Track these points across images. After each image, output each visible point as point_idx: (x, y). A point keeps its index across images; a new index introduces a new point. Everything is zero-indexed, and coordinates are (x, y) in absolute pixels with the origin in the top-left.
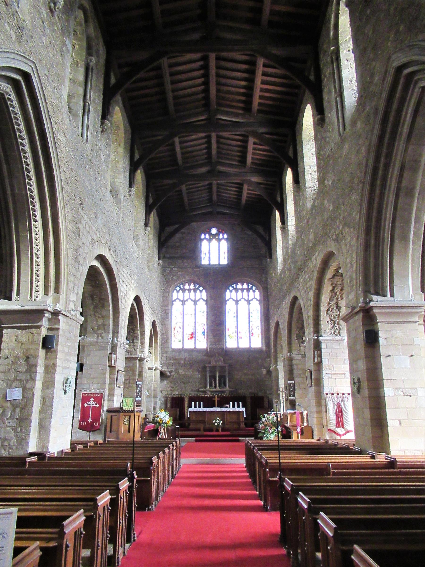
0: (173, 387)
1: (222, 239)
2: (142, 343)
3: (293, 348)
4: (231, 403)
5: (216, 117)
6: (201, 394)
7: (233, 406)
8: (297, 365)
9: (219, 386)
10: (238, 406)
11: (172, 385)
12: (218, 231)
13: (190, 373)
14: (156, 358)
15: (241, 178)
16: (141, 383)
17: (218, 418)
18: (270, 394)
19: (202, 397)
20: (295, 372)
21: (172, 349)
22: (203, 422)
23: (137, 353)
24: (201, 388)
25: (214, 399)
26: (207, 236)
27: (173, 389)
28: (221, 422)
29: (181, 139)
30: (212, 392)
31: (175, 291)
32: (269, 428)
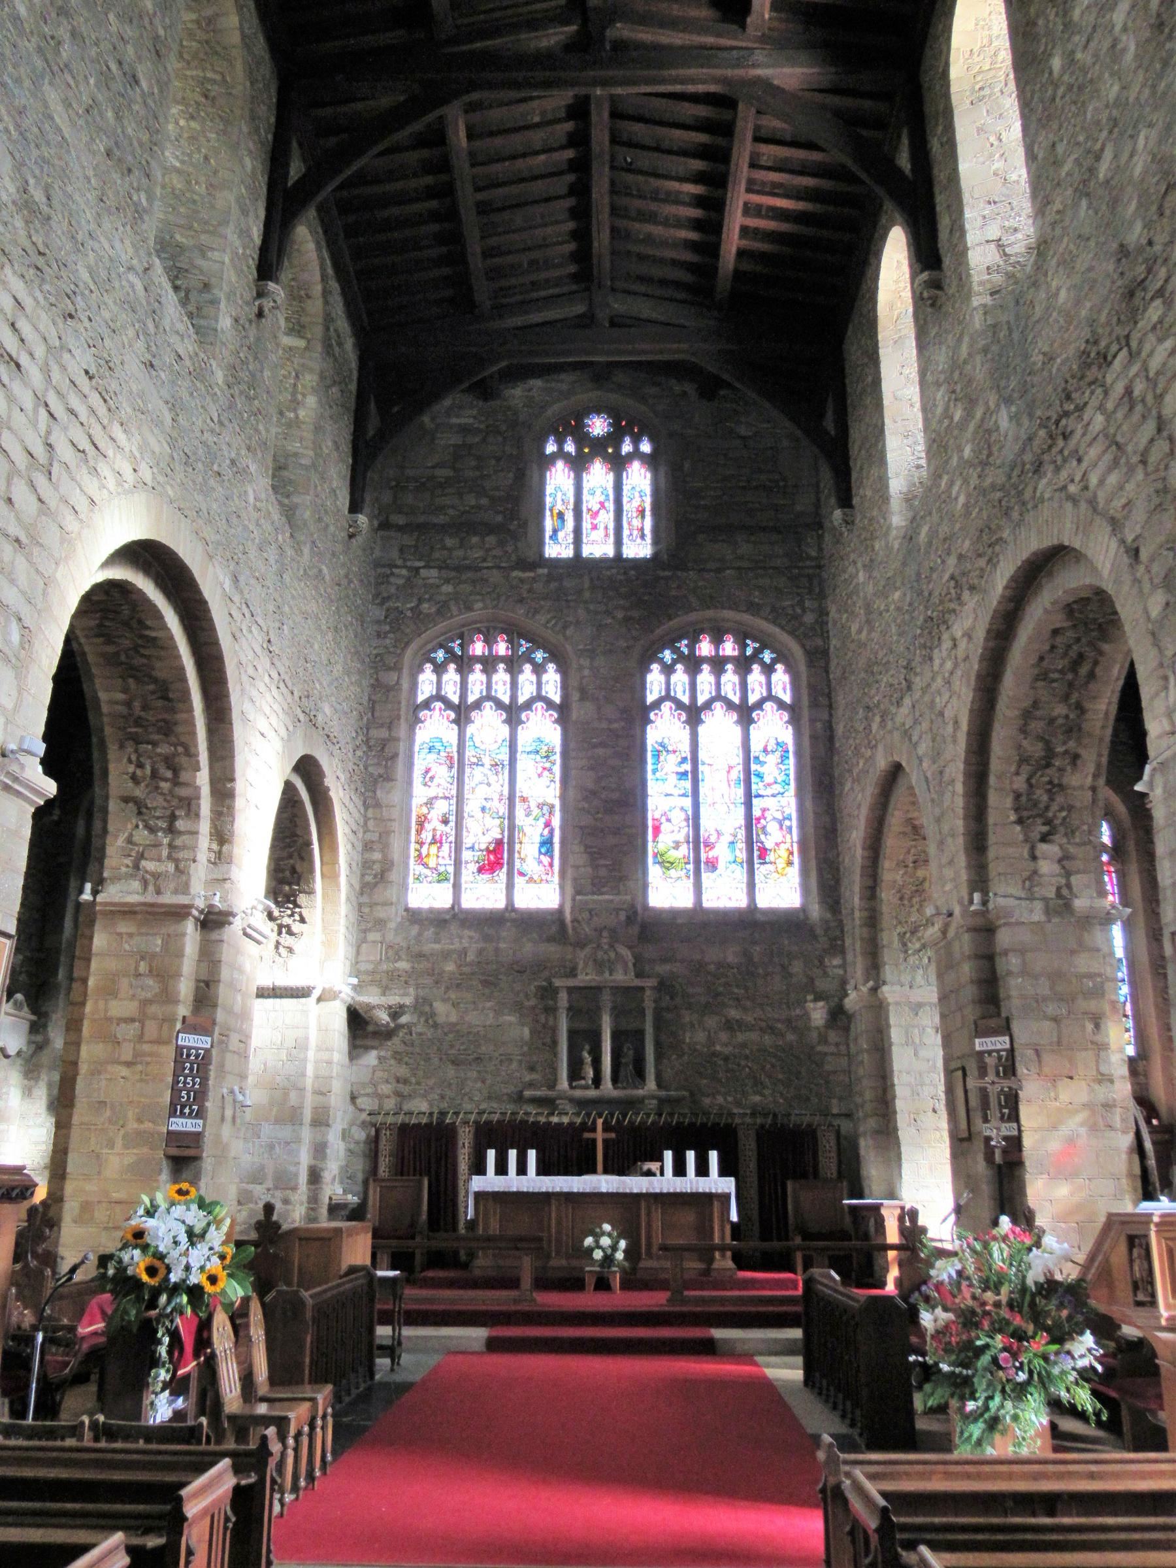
0: (406, 1082)
1: (630, 457)
2: (222, 836)
3: (994, 869)
4: (668, 1155)
5: (610, 33)
6: (535, 1115)
7: (680, 1170)
8: (1022, 951)
9: (615, 1080)
10: (703, 1170)
11: (403, 1071)
12: (616, 424)
13: (480, 1017)
14: (328, 944)
15: (718, 72)
16: (203, 1042)
17: (607, 1227)
18: (848, 1116)
19: (536, 1123)
20: (1015, 989)
21: (407, 910)
22: (531, 1243)
23: (187, 885)
24: (531, 1085)
25: (587, 1135)
26: (570, 447)
27: (406, 1090)
28: (623, 1244)
29: (476, 117)
30: (582, 1104)
31: (428, 667)
32: (999, 1341)
